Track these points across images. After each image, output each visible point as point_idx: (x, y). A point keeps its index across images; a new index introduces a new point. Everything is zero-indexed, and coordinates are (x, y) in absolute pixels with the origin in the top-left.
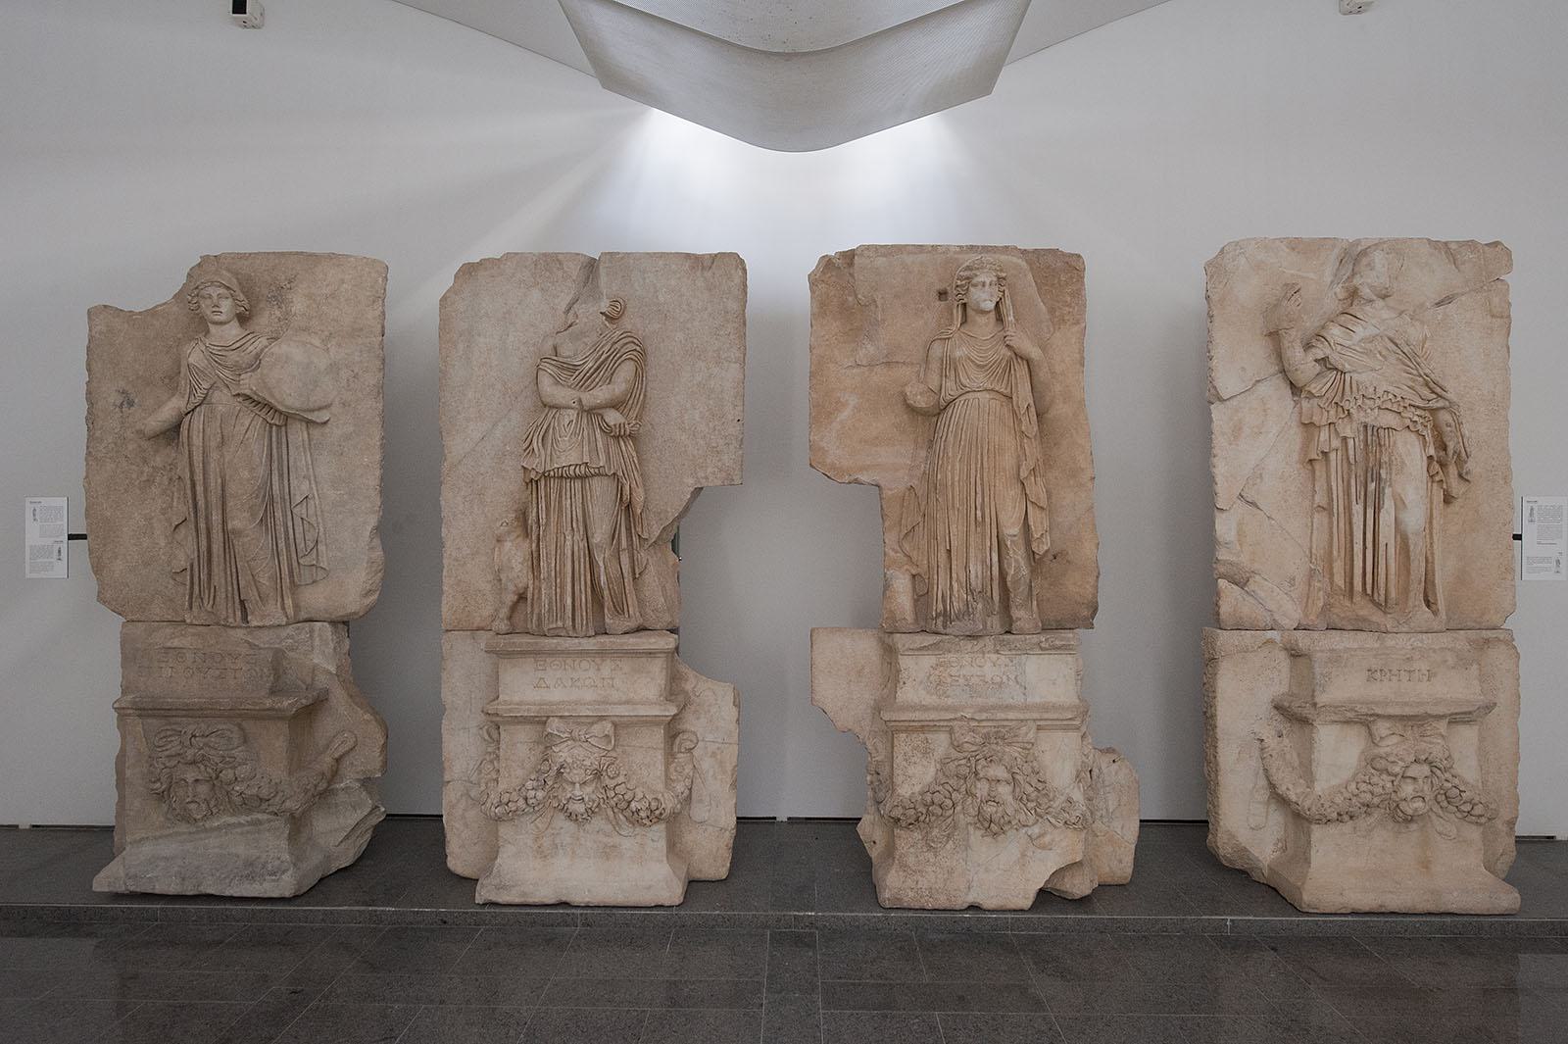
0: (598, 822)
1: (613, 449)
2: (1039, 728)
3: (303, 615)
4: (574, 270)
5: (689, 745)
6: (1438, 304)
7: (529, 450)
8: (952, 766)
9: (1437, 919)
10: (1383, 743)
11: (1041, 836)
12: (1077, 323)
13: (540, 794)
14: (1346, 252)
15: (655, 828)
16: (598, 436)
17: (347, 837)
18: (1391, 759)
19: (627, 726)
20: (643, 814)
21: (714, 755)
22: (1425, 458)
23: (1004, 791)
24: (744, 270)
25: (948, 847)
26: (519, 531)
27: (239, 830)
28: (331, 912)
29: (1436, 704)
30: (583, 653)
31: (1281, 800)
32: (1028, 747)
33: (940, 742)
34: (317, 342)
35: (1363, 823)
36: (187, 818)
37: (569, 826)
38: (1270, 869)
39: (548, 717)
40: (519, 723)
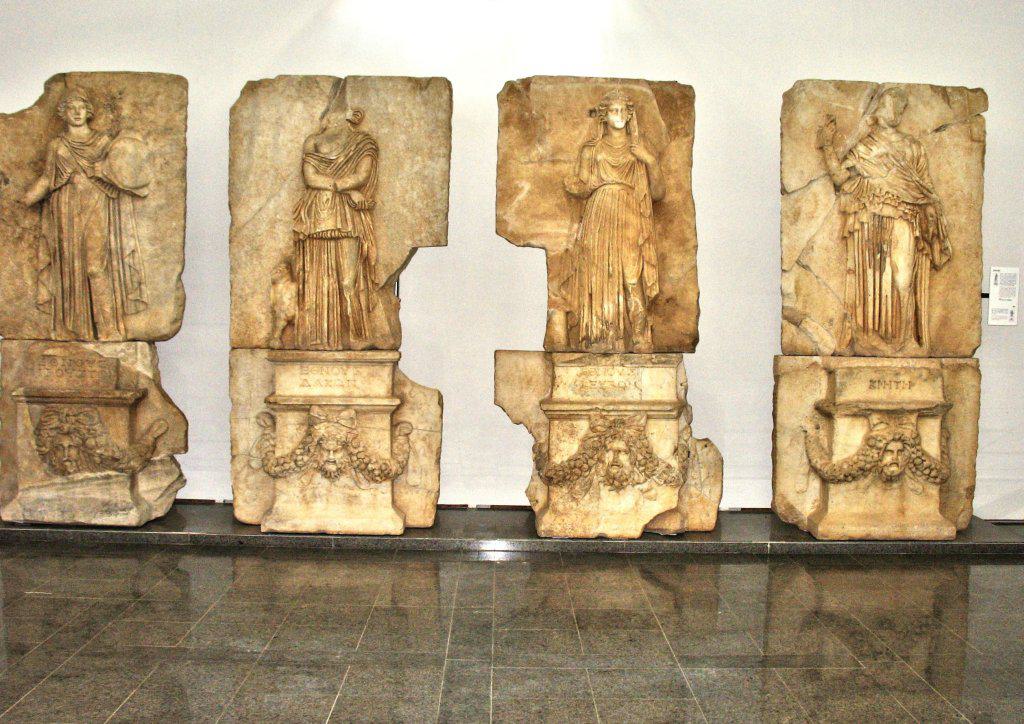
0: (344, 480)
1: (357, 219)
2: (648, 417)
3: (130, 336)
4: (328, 88)
5: (406, 431)
6: (937, 130)
7: (298, 219)
8: (589, 442)
9: (901, 543)
10: (876, 429)
11: (648, 490)
12: (687, 135)
13: (306, 458)
14: (875, 91)
15: (384, 484)
16: (347, 211)
17: (161, 496)
18: (879, 438)
19: (365, 413)
20: (377, 472)
21: (424, 439)
22: (912, 238)
23: (624, 458)
24: (451, 91)
25: (585, 498)
26: (288, 277)
27: (96, 482)
28: (165, 535)
29: (910, 403)
30: (336, 361)
31: (814, 470)
32: (642, 432)
33: (583, 426)
34: (139, 138)
35: (863, 483)
36: (64, 472)
37: (325, 482)
38: (809, 519)
39: (311, 405)
40: (290, 410)
